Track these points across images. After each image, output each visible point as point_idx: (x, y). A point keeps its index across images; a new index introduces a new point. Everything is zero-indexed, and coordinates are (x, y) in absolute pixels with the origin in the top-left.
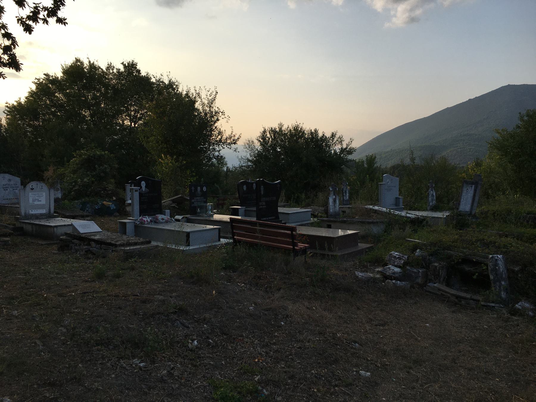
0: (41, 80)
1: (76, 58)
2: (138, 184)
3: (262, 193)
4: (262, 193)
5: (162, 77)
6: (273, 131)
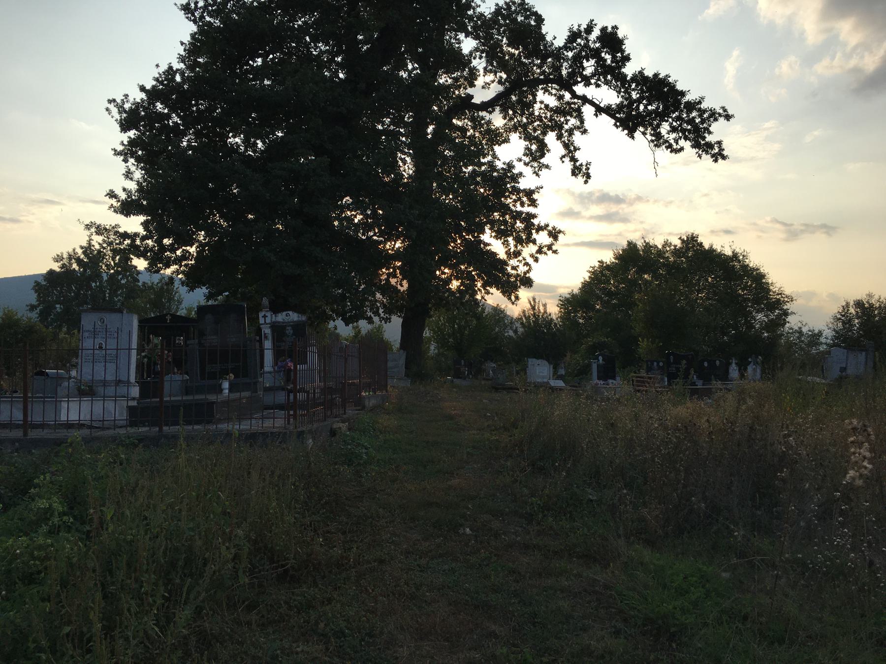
0: (596, 269)
1: (628, 241)
2: (597, 358)
3: (672, 361)
4: (672, 361)
5: (724, 249)
6: (859, 304)
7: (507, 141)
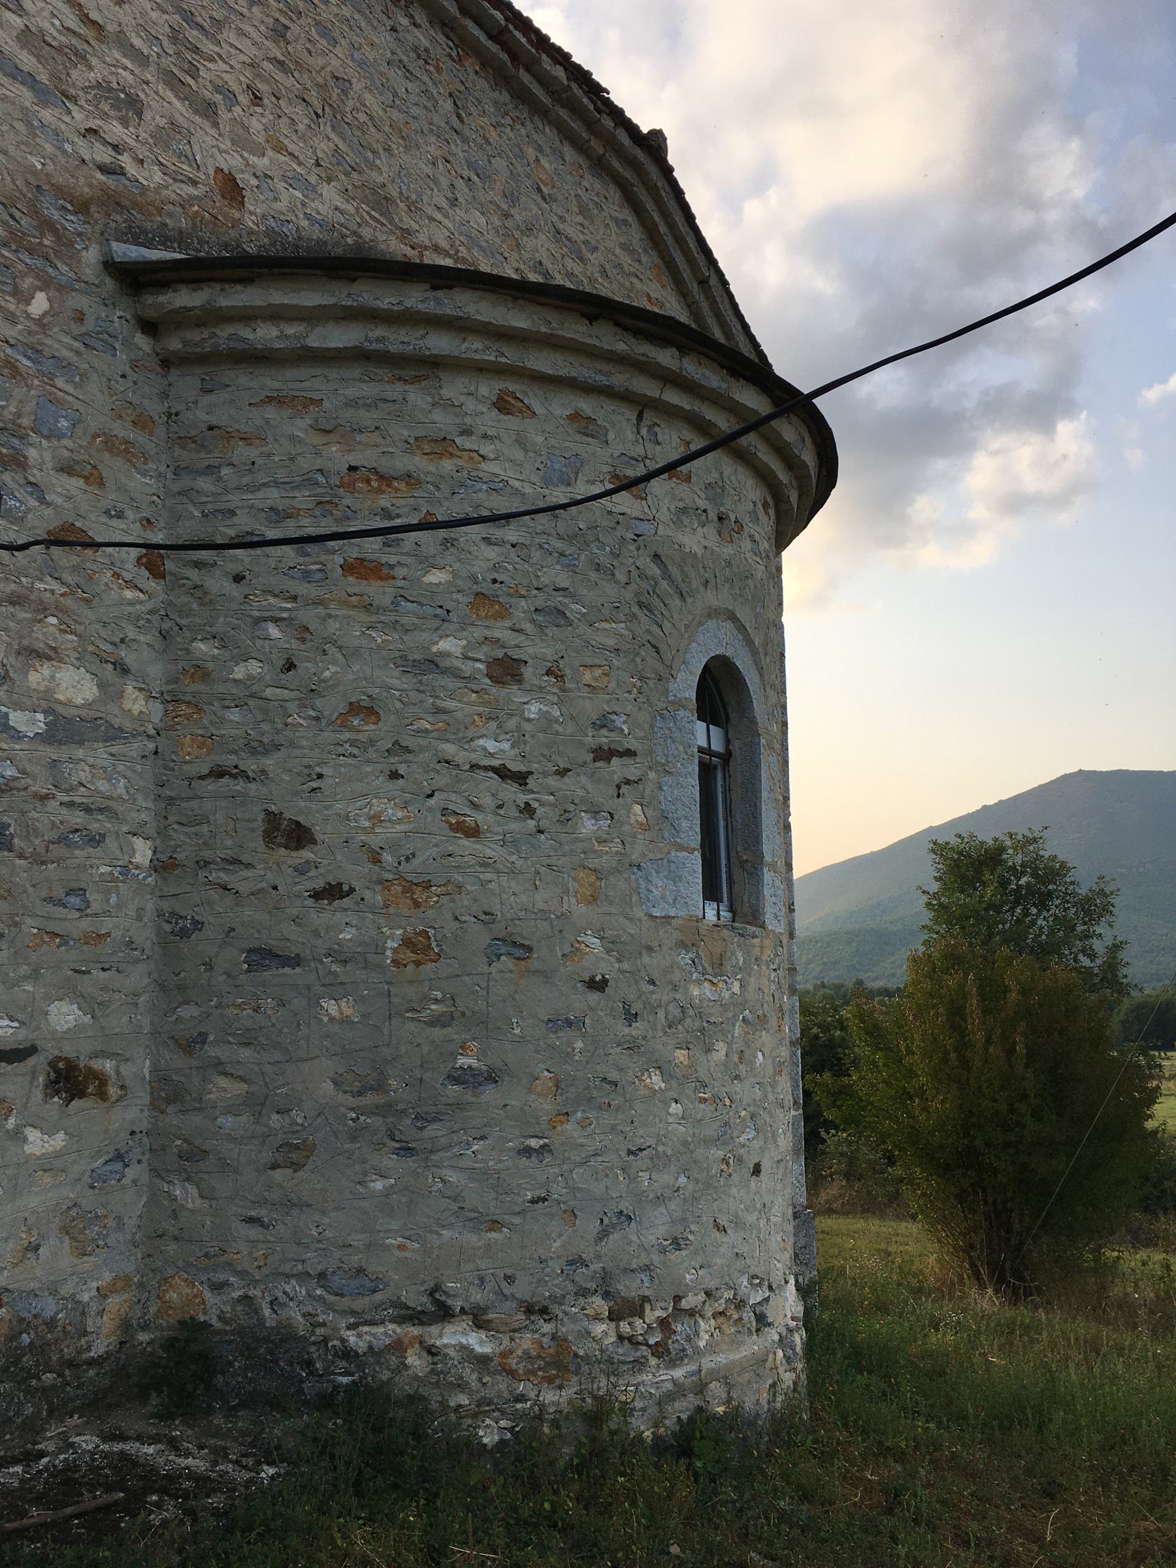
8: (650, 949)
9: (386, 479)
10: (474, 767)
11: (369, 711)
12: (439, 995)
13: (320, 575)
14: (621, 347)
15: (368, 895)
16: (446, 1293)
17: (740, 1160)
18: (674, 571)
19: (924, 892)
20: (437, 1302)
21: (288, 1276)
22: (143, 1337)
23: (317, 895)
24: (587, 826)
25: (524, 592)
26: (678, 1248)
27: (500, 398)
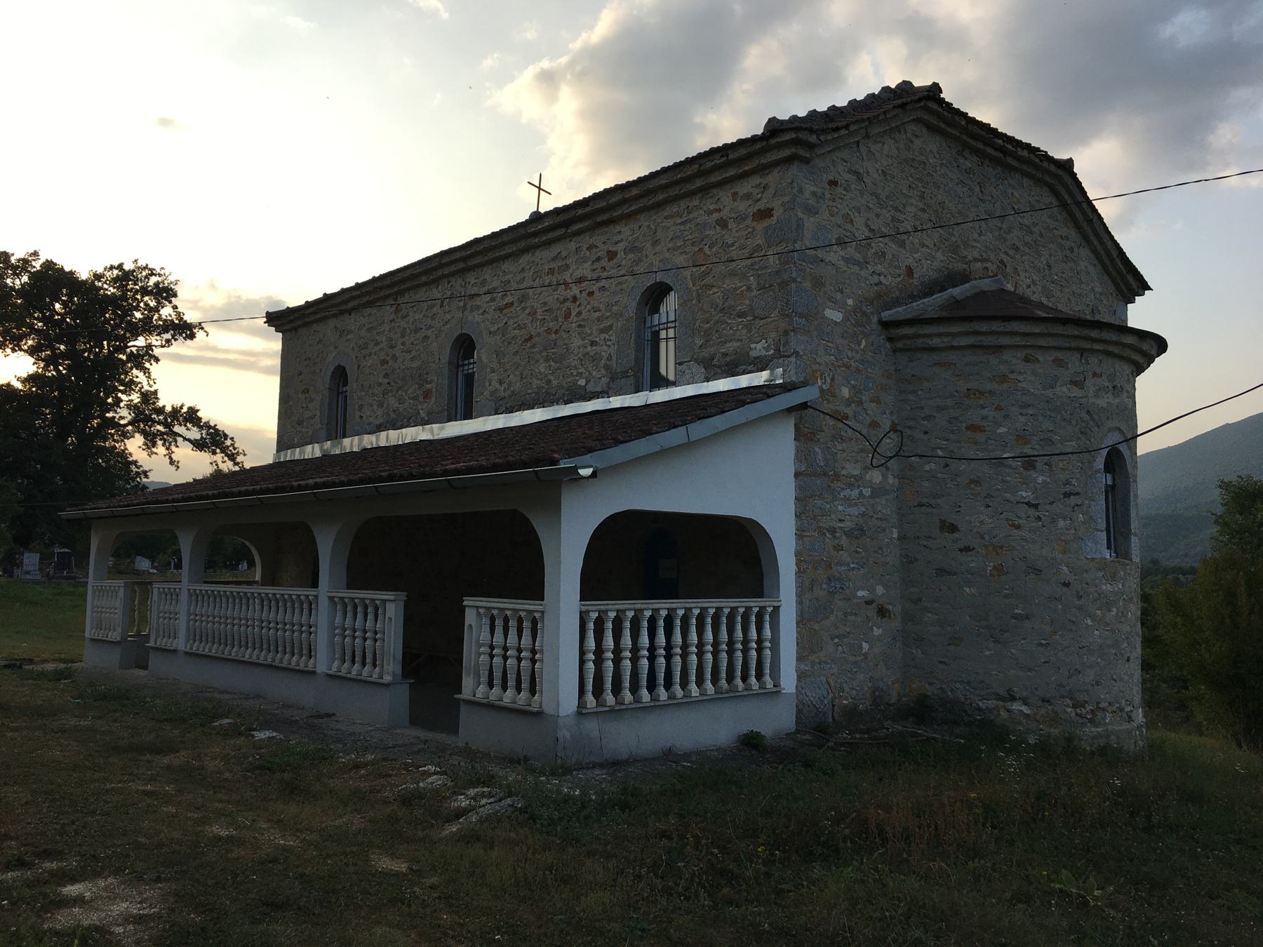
7: (133, 437)
8: (1087, 572)
9: (982, 393)
10: (1018, 503)
11: (977, 482)
12: (1007, 587)
13: (957, 431)
14: (1076, 333)
15: (980, 550)
16: (1013, 691)
17: (1122, 655)
18: (1096, 417)
19: (1213, 514)
20: (1010, 695)
21: (956, 682)
22: (904, 699)
23: (961, 550)
24: (1061, 523)
25: (1036, 433)
26: (1098, 685)
27: (1026, 357)
